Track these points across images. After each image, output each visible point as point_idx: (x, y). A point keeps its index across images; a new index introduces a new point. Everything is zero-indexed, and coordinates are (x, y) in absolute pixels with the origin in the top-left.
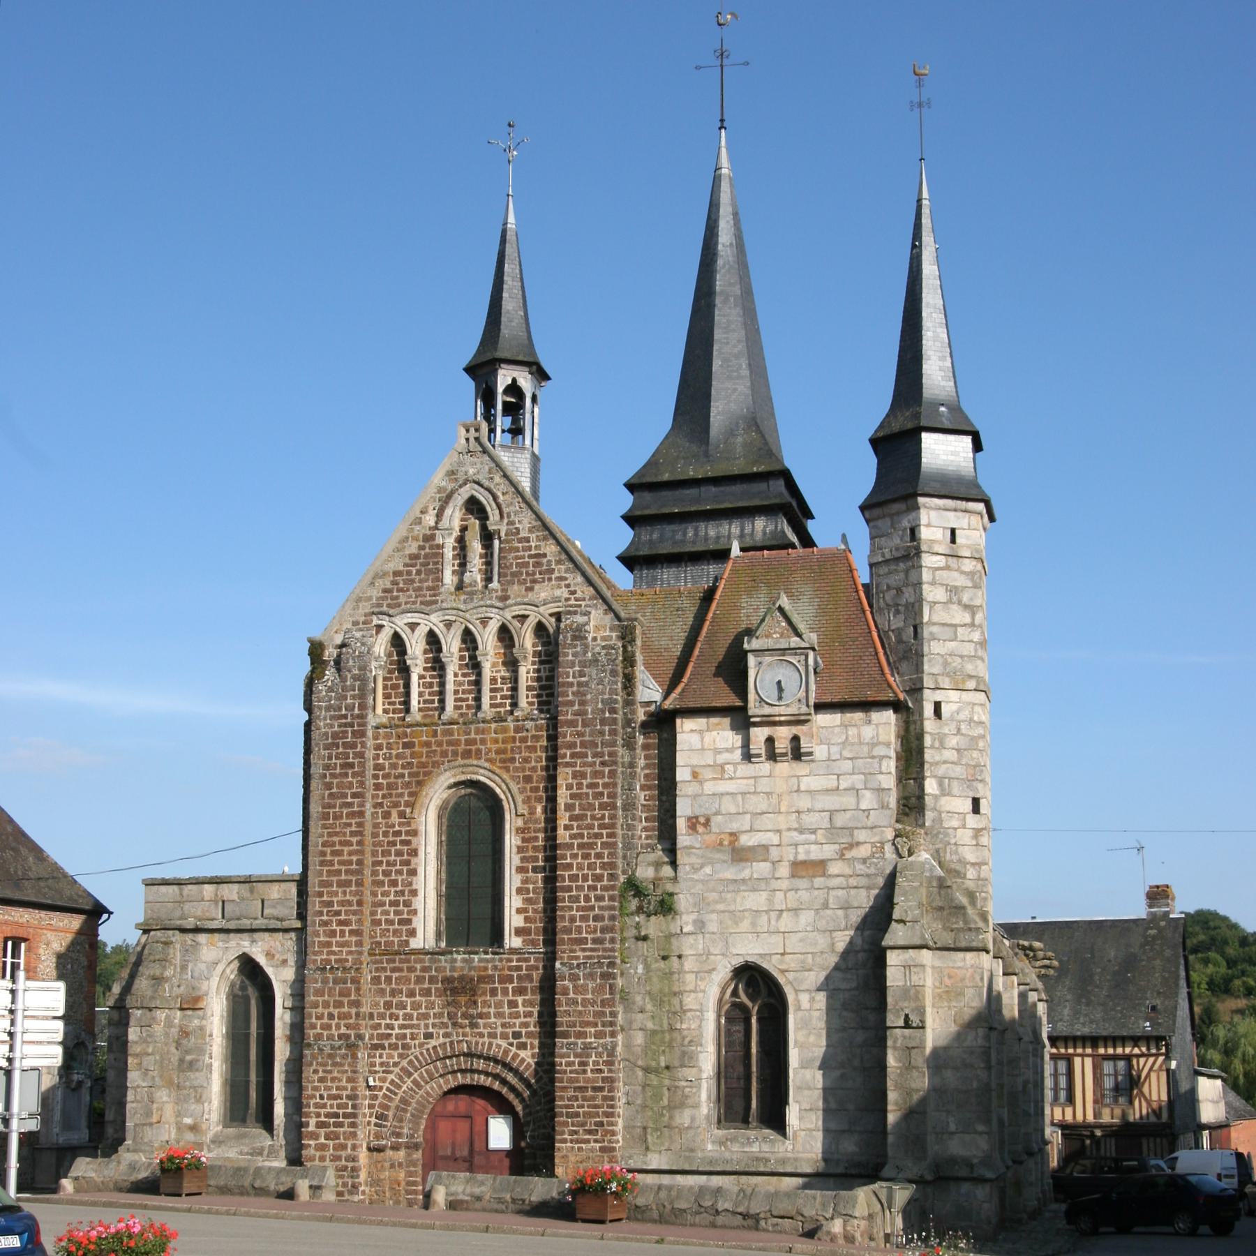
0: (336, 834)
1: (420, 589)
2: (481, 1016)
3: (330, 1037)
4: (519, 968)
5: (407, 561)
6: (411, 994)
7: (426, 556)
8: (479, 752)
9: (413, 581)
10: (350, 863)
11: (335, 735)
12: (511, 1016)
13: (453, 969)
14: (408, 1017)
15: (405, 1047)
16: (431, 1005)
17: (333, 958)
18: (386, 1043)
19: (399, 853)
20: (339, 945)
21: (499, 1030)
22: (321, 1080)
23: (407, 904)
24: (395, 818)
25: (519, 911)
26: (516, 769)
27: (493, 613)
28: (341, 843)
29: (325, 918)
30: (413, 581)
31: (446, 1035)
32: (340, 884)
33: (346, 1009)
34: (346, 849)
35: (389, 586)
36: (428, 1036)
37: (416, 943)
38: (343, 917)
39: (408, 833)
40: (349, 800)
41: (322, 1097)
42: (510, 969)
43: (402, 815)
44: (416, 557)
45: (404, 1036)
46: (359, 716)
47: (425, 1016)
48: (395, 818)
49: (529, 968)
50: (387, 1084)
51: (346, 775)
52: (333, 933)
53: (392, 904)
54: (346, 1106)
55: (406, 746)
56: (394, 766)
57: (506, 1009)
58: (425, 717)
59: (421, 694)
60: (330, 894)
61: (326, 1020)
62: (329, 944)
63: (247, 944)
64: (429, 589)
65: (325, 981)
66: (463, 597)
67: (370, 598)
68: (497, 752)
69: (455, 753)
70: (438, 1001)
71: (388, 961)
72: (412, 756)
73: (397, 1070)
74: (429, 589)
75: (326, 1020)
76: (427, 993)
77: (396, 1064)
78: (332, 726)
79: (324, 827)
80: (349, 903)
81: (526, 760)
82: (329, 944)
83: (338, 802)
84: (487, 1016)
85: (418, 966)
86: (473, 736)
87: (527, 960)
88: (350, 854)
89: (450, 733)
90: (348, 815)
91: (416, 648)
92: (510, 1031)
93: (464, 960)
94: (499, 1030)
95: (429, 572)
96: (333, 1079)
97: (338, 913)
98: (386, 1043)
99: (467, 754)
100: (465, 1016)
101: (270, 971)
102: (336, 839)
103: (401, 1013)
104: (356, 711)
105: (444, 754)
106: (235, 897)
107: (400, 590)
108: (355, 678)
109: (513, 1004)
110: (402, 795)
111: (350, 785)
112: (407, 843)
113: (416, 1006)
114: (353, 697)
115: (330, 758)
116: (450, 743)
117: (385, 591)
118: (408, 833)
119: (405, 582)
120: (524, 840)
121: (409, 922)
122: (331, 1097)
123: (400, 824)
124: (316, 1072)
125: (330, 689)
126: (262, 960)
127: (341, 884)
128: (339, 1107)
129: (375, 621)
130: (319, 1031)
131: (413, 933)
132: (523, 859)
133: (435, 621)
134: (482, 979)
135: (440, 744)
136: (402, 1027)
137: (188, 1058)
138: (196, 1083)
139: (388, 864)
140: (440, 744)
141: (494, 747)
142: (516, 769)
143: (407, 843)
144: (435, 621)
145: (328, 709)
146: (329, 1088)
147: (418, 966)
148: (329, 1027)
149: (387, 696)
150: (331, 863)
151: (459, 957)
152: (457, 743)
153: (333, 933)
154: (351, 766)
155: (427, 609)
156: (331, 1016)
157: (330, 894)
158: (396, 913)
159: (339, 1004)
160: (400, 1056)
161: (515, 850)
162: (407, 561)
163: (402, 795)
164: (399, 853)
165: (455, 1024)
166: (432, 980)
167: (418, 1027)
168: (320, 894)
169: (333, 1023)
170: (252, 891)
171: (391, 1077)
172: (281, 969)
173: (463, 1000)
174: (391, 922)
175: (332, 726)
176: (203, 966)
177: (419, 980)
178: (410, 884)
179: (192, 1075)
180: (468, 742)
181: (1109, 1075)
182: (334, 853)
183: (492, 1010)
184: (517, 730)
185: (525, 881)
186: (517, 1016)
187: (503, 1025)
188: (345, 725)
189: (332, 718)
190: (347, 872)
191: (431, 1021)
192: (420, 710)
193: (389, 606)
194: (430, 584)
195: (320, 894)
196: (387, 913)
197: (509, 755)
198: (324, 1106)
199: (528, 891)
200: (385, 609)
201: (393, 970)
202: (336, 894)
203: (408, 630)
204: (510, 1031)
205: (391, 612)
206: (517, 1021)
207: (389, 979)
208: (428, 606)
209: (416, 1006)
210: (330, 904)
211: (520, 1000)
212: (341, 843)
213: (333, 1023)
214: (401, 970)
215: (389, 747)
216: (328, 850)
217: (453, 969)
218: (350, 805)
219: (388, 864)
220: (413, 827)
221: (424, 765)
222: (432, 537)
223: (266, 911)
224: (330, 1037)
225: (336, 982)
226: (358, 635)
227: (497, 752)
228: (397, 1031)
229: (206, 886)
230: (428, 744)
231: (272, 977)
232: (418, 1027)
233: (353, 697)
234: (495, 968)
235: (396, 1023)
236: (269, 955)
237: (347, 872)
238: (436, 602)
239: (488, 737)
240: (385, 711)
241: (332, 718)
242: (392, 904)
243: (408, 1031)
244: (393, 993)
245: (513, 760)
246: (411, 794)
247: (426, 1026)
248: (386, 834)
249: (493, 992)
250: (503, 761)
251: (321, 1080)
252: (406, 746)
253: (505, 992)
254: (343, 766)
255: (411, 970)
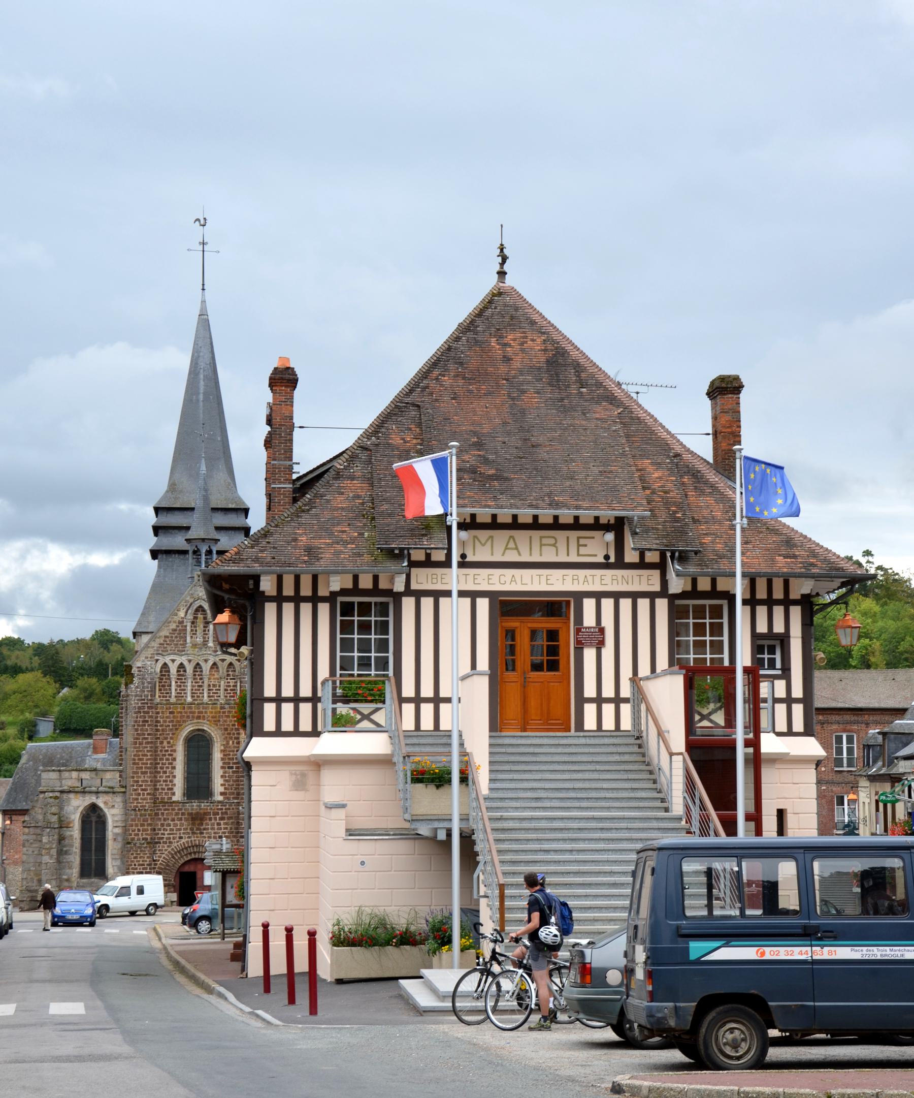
0: (141, 751)
1: (177, 644)
2: (204, 829)
3: (139, 839)
4: (222, 809)
5: (171, 631)
6: (173, 820)
7: (180, 630)
8: (204, 716)
9: (174, 641)
10: (147, 764)
11: (139, 707)
12: (218, 829)
13: (192, 809)
14: (172, 830)
15: (170, 842)
16: (182, 825)
17: (139, 805)
18: (162, 841)
19: (168, 759)
20: (141, 799)
21: (213, 835)
22: (135, 858)
23: (171, 781)
24: (165, 744)
25: (222, 785)
26: (221, 725)
27: (160, 658)
28: (142, 755)
29: (135, 787)
30: (174, 641)
31: (189, 837)
32: (142, 773)
33: (146, 827)
34: (145, 758)
35: (162, 642)
36: (181, 838)
37: (175, 798)
38: (144, 787)
39: (171, 751)
40: (146, 736)
41: (135, 865)
42: (218, 809)
43: (169, 743)
44: (175, 630)
45: (170, 838)
46: (151, 700)
47: (180, 830)
48: (165, 744)
49: (226, 809)
50: (161, 859)
51: (145, 725)
52: (139, 794)
53: (164, 781)
54: (146, 869)
55: (170, 713)
56: (165, 721)
57: (216, 827)
58: (177, 700)
59: (176, 690)
60: (138, 777)
61: (136, 832)
62: (137, 799)
63: (94, 798)
64: (181, 645)
65: (136, 815)
66: (197, 650)
67: (153, 647)
68: (212, 717)
69: (193, 717)
70: (185, 823)
71: (163, 806)
72: (174, 717)
73: (166, 852)
74: (181, 645)
75: (136, 832)
76: (181, 819)
77: (166, 850)
78: (138, 704)
79: (135, 748)
80: (147, 781)
81: (225, 721)
82: (137, 799)
83: (141, 737)
84: (208, 829)
85: (176, 808)
86: (201, 710)
87: (225, 806)
88: (147, 760)
89: (190, 708)
90: (146, 743)
91: (173, 669)
92: (217, 835)
93: (197, 806)
94: (213, 835)
95: (181, 637)
96: (140, 857)
97: (142, 786)
98: (162, 841)
99: (198, 718)
100: (197, 829)
101: (106, 810)
102: (140, 753)
103: (168, 828)
104: (149, 698)
105: (188, 717)
106: (88, 777)
107: (167, 644)
108: (149, 683)
109: (219, 824)
110: (169, 734)
111: (147, 730)
112: (171, 755)
113: (175, 825)
114: (148, 691)
115: (137, 718)
116: (191, 712)
117: (160, 644)
118: (171, 751)
119: (170, 641)
120: (224, 755)
121: (172, 789)
122: (139, 865)
123: (168, 747)
124: (132, 854)
125: (137, 687)
126: (102, 805)
127: (143, 773)
128: (143, 869)
129: (156, 658)
130: (133, 836)
131: (174, 794)
132: (224, 763)
133: (184, 660)
134: (205, 814)
135: (186, 713)
136: (168, 834)
137: (65, 849)
138: (69, 860)
139: (162, 764)
140: (186, 713)
141: (211, 715)
142: (221, 725)
143: (171, 755)
144: (184, 660)
145: (136, 696)
146: (139, 861)
147: (176, 808)
148: (138, 835)
149: (160, 690)
150: (138, 764)
151: (195, 804)
152: (194, 713)
153: (139, 794)
154: (147, 721)
155: (164, 653)
156: (139, 830)
157: (138, 777)
158: (166, 785)
159: (142, 825)
160: (168, 846)
161: (220, 759)
162: (171, 631)
163: (169, 734)
164: (168, 759)
165: (193, 833)
166: (183, 814)
167: (176, 834)
168: (133, 777)
169: (140, 833)
170: (96, 775)
171: (163, 855)
172: (111, 810)
173: (197, 822)
174: (163, 789)
175: (138, 704)
176: (72, 808)
177: (177, 814)
178: (173, 773)
179: (67, 857)
180: (199, 712)
181: (60, 779)
182: (140, 759)
183: (209, 827)
184: (221, 708)
185: (225, 772)
186: (221, 829)
187: (215, 833)
188: (144, 703)
189: (138, 700)
190: (145, 768)
191: (182, 831)
192: (176, 697)
193: (162, 651)
194: (181, 642)
195: (133, 777)
196: (162, 785)
197: (217, 719)
198: (136, 869)
199: (226, 777)
200: (160, 652)
201: (165, 810)
202: (140, 777)
203: (171, 662)
204: (217, 835)
205: (164, 653)
206: (221, 831)
207: (163, 814)
208: (181, 652)
209: (175, 825)
210: (138, 782)
211: (222, 822)
212: (142, 755)
213: (140, 833)
214: (169, 810)
215: (163, 713)
216: (137, 758)
217: (192, 809)
218: (147, 738)
219: (162, 764)
220: (174, 748)
221: (178, 722)
222: (182, 622)
223: (103, 785)
224: (139, 839)
225: (141, 815)
226: (149, 663)
227: (212, 717)
228: (166, 836)
229: (73, 772)
230: (181, 713)
231: (107, 813)
232: (176, 834)
233: (148, 691)
234: (211, 809)
235: (166, 832)
236: (106, 803)
237: (145, 768)
238: (184, 651)
239: (208, 711)
240: (160, 697)
241: (138, 700)
242: (164, 781)
243: (171, 836)
244: (165, 820)
245: (219, 721)
246: (173, 734)
247: (180, 834)
248: (161, 751)
249: (210, 819)
250: (215, 721)
251: (135, 858)
252: (170, 713)
253: (215, 819)
254: (143, 721)
255: (173, 810)
